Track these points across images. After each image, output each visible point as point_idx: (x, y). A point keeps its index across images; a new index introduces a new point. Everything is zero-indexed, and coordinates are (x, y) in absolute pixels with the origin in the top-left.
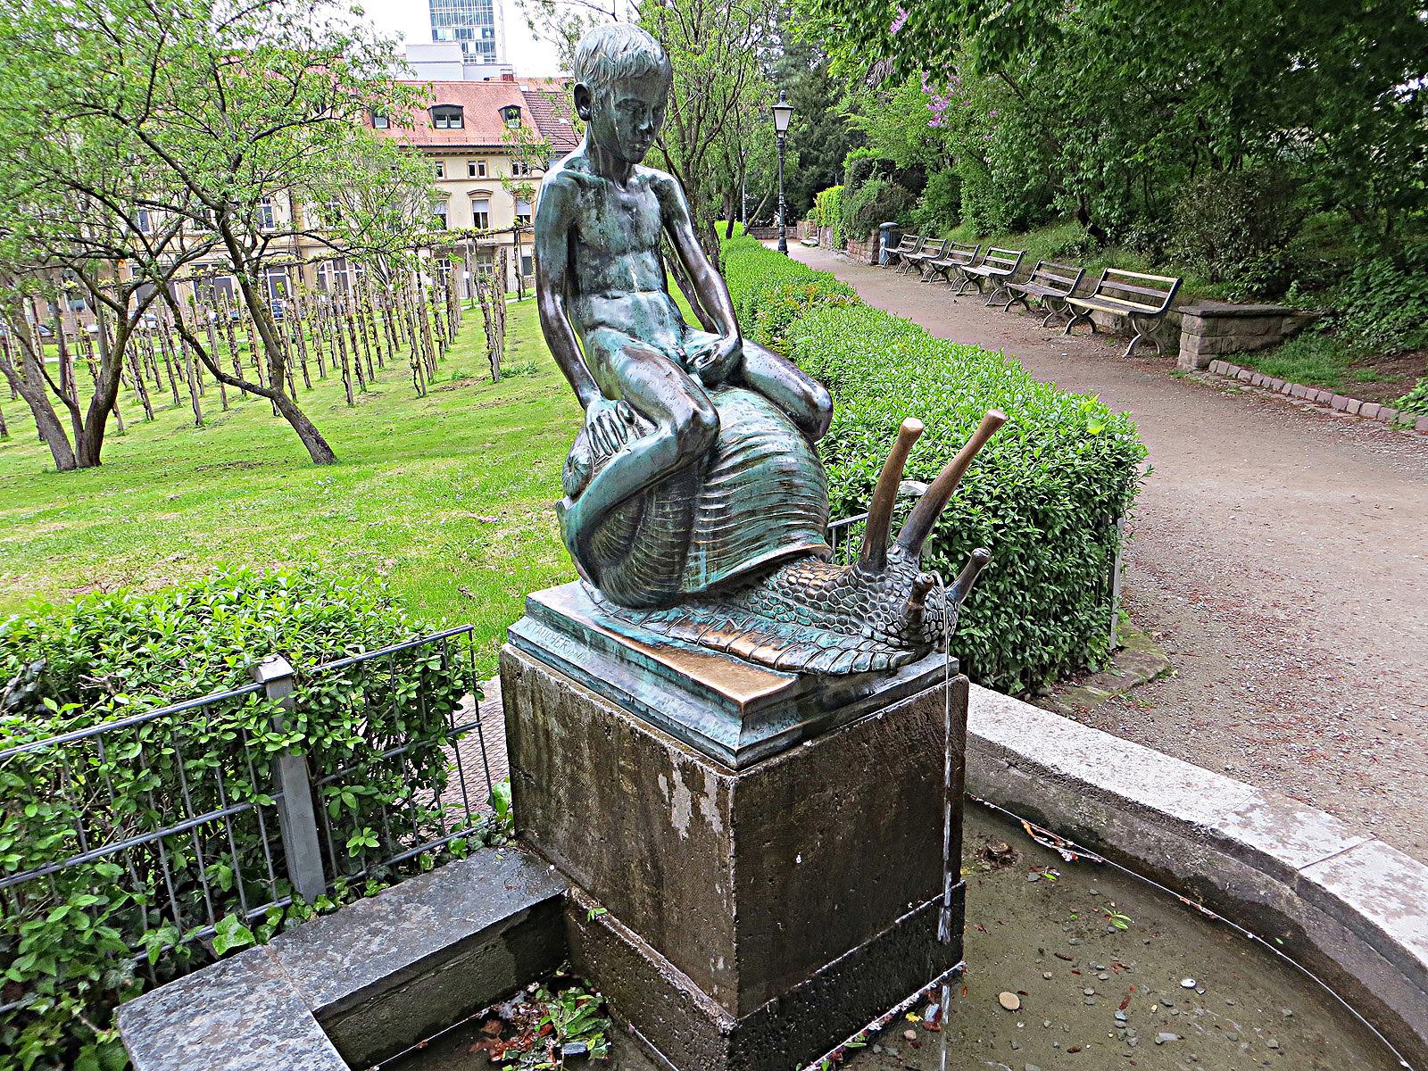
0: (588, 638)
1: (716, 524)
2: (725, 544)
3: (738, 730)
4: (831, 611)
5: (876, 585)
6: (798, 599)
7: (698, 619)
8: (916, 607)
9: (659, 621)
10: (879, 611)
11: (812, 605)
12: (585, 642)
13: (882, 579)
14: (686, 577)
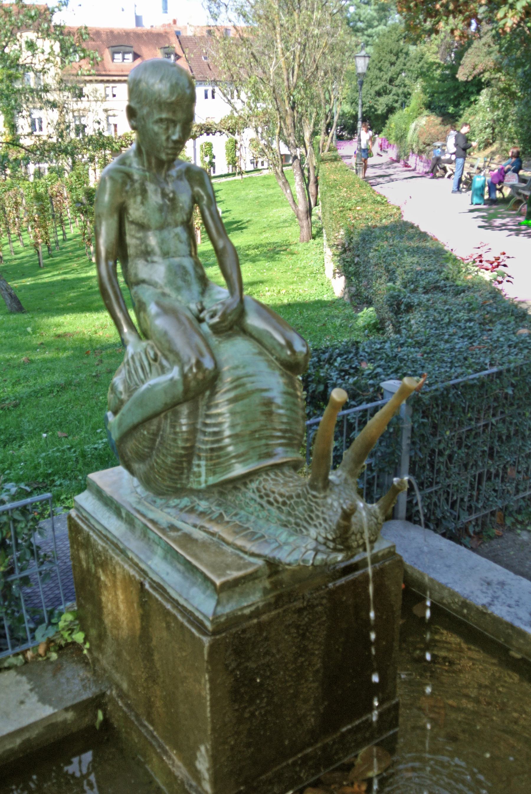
0: (124, 515)
1: (213, 442)
2: (219, 457)
3: (345, 507)
4: (289, 514)
5: (319, 501)
6: (269, 503)
7: (201, 509)
8: (346, 523)
9: (175, 507)
10: (322, 522)
11: (279, 508)
12: (122, 518)
13: (325, 497)
14: (192, 478)
